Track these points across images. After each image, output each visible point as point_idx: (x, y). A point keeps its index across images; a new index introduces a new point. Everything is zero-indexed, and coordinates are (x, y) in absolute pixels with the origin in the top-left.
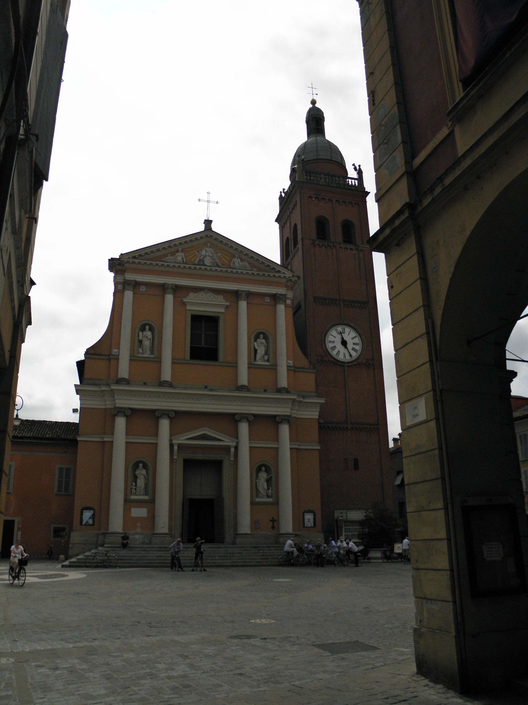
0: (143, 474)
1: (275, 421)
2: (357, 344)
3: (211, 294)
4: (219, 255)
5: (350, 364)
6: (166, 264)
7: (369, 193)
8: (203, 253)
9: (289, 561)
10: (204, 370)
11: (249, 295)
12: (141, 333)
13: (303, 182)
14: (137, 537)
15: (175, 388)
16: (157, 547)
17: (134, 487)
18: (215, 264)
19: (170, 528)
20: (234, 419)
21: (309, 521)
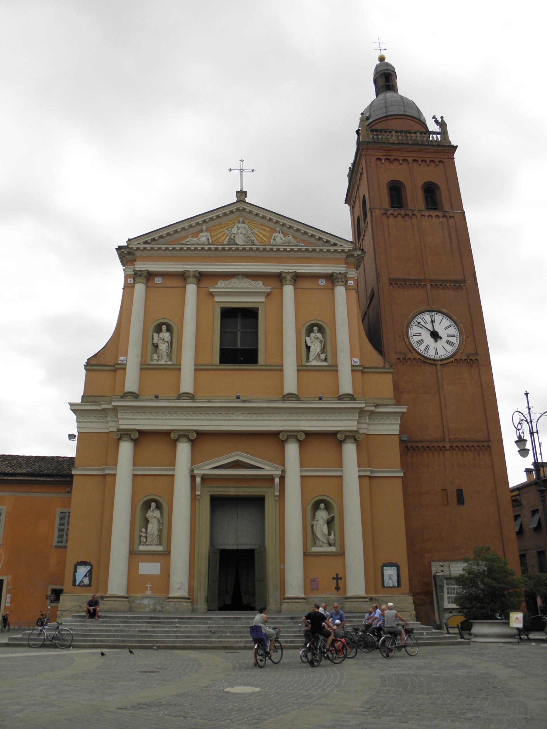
0: (156, 517)
1: (335, 439)
2: (453, 335)
3: (246, 280)
5: (445, 362)
6: (185, 247)
7: (457, 146)
8: (235, 230)
10: (239, 377)
11: (297, 277)
12: (156, 335)
13: (368, 142)
14: (146, 601)
16: (146, 618)
17: (143, 535)
18: (250, 242)
19: (191, 589)
20: (276, 439)
21: (390, 579)
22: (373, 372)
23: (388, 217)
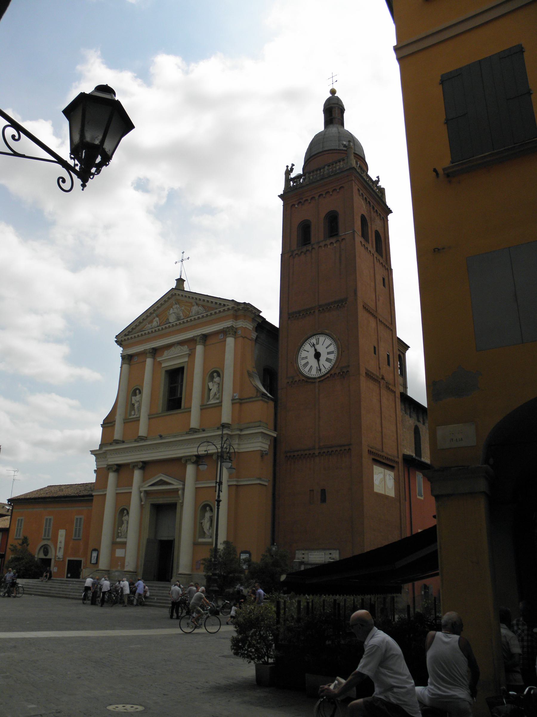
4: (183, 308)
5: (322, 378)
7: (279, 196)
9: (94, 597)
10: (174, 419)
14: (117, 574)
15: (164, 438)
19: (137, 567)
20: (179, 462)
22: (251, 402)
23: (294, 258)
